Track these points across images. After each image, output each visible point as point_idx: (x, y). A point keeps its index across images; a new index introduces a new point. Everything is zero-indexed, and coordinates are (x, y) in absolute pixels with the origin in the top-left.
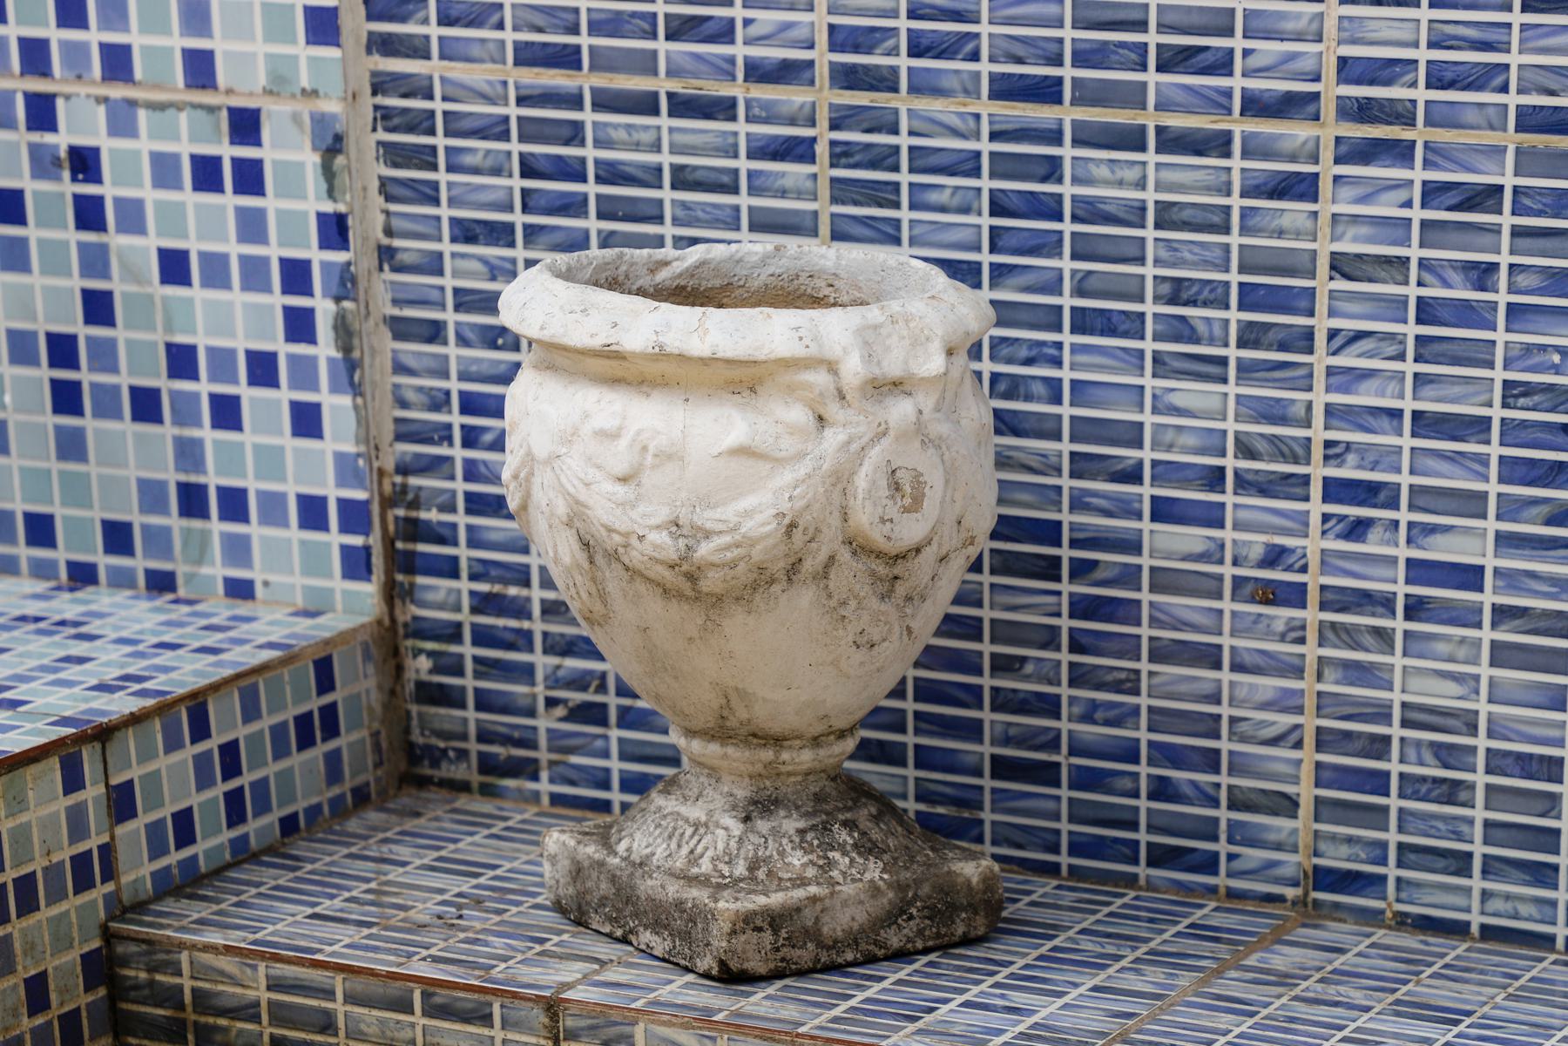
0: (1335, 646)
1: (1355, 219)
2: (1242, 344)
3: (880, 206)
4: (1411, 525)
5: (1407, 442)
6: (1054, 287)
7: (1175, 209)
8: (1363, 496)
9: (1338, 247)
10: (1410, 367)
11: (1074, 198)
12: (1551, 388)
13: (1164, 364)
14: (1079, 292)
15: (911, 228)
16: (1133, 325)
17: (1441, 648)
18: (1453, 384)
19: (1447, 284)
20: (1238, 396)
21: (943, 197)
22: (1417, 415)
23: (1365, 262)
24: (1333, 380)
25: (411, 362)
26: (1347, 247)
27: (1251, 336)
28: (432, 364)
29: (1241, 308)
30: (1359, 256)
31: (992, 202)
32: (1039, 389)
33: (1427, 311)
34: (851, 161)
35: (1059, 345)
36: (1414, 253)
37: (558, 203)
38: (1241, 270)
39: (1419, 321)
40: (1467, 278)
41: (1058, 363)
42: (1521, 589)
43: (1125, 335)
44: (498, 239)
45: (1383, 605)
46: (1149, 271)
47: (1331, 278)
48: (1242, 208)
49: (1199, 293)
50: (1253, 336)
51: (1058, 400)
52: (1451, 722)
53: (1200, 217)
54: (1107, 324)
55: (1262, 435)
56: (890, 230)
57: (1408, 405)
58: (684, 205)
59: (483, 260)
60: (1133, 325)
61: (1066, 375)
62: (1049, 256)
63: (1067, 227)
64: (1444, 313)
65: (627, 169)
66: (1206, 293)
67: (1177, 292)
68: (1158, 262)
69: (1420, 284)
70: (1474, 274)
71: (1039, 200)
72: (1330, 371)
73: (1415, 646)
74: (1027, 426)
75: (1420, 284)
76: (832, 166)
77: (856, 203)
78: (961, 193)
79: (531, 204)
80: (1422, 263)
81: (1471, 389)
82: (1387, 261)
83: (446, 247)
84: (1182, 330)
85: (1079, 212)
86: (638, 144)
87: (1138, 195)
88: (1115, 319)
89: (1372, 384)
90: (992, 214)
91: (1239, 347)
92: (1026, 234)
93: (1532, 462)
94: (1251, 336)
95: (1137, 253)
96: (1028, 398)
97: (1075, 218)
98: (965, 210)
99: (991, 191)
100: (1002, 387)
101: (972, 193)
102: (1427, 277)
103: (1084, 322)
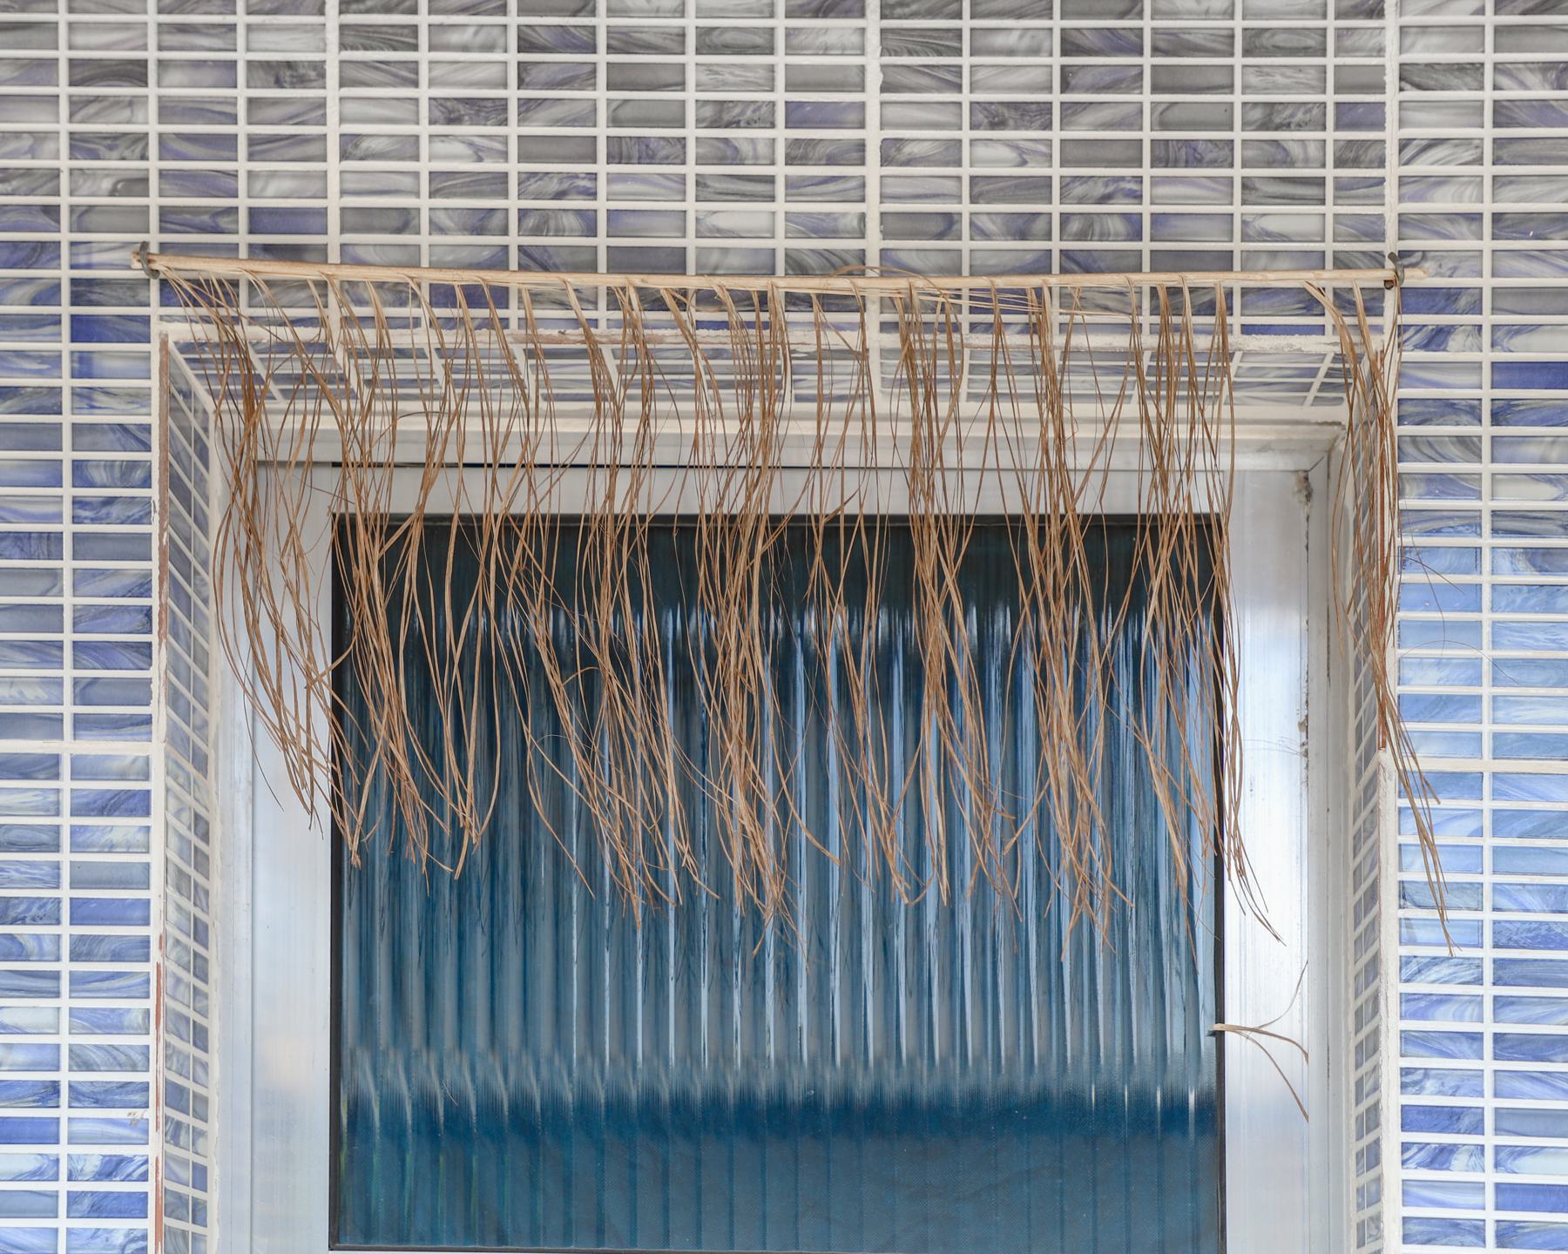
0: (1416, 460)
1: (1424, 29)
2: (790, 160)
3: (939, 54)
4: (1495, 327)
5: (1487, 244)
6: (1133, 121)
7: (1267, 35)
8: (1442, 303)
9: (1409, 58)
10: (1488, 170)
11: (1155, 31)
12: (28, 172)
13: (1256, 189)
14: (615, 121)
15: (971, 74)
16: (1222, 154)
17: (1533, 450)
18: (1534, 183)
19: (1524, 86)
20: (1336, 215)
21: (1011, 40)
22: (1497, 218)
23: (1436, 71)
24: (1405, 189)
25: (362, 253)
26: (1418, 56)
27: (798, 154)
28: (941, 260)
29: (1338, 127)
30: (1430, 66)
31: (1063, 40)
32: (570, 221)
33: (1503, 113)
34: (907, 10)
35: (1139, 179)
36: (1489, 57)
37: (1108, 79)
38: (1339, 89)
39: (1496, 124)
40: (1545, 79)
41: (1138, 197)
42: (13, 370)
43: (1213, 163)
44: (487, 119)
45: (1467, 413)
46: (1237, 98)
47: (1401, 90)
48: (1337, 29)
49: (742, 113)
50: (1352, 155)
51: (1138, 236)
52: (1536, 526)
53: (1295, 41)
54: (1193, 155)
55: (1363, 253)
56: (949, 77)
57: (1487, 208)
58: (709, 68)
59: (1011, 144)
60: (1222, 154)
61: (1146, 209)
62: (1128, 91)
63: (1147, 61)
64: (1522, 115)
65: (644, 36)
66: (749, 113)
67: (720, 115)
68: (700, 87)
69: (1496, 87)
70: (1553, 75)
71: (570, 33)
72: (1403, 181)
73: (1505, 451)
74: (557, 260)
75: (1496, 87)
76: (883, 17)
77: (910, 53)
78: (485, 30)
79: (1073, 82)
80: (1498, 68)
81: (1554, 187)
82: (1461, 68)
83: (424, 129)
84: (728, 153)
85: (1162, 45)
86: (658, 11)
87: (677, 22)
88: (1201, 147)
89: (1448, 190)
90: (1064, 53)
91: (1336, 166)
92: (556, 68)
93: (15, 245)
94: (798, 154)
95: (678, 79)
96: (559, 232)
97: (611, 49)
98: (1035, 51)
99: (1063, 30)
100: (1075, 226)
101: (1042, 34)
102: (1504, 80)
103: (1165, 155)
